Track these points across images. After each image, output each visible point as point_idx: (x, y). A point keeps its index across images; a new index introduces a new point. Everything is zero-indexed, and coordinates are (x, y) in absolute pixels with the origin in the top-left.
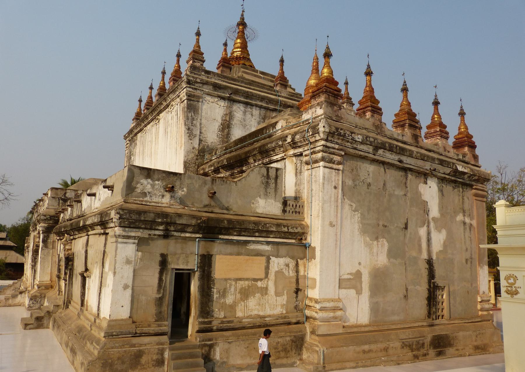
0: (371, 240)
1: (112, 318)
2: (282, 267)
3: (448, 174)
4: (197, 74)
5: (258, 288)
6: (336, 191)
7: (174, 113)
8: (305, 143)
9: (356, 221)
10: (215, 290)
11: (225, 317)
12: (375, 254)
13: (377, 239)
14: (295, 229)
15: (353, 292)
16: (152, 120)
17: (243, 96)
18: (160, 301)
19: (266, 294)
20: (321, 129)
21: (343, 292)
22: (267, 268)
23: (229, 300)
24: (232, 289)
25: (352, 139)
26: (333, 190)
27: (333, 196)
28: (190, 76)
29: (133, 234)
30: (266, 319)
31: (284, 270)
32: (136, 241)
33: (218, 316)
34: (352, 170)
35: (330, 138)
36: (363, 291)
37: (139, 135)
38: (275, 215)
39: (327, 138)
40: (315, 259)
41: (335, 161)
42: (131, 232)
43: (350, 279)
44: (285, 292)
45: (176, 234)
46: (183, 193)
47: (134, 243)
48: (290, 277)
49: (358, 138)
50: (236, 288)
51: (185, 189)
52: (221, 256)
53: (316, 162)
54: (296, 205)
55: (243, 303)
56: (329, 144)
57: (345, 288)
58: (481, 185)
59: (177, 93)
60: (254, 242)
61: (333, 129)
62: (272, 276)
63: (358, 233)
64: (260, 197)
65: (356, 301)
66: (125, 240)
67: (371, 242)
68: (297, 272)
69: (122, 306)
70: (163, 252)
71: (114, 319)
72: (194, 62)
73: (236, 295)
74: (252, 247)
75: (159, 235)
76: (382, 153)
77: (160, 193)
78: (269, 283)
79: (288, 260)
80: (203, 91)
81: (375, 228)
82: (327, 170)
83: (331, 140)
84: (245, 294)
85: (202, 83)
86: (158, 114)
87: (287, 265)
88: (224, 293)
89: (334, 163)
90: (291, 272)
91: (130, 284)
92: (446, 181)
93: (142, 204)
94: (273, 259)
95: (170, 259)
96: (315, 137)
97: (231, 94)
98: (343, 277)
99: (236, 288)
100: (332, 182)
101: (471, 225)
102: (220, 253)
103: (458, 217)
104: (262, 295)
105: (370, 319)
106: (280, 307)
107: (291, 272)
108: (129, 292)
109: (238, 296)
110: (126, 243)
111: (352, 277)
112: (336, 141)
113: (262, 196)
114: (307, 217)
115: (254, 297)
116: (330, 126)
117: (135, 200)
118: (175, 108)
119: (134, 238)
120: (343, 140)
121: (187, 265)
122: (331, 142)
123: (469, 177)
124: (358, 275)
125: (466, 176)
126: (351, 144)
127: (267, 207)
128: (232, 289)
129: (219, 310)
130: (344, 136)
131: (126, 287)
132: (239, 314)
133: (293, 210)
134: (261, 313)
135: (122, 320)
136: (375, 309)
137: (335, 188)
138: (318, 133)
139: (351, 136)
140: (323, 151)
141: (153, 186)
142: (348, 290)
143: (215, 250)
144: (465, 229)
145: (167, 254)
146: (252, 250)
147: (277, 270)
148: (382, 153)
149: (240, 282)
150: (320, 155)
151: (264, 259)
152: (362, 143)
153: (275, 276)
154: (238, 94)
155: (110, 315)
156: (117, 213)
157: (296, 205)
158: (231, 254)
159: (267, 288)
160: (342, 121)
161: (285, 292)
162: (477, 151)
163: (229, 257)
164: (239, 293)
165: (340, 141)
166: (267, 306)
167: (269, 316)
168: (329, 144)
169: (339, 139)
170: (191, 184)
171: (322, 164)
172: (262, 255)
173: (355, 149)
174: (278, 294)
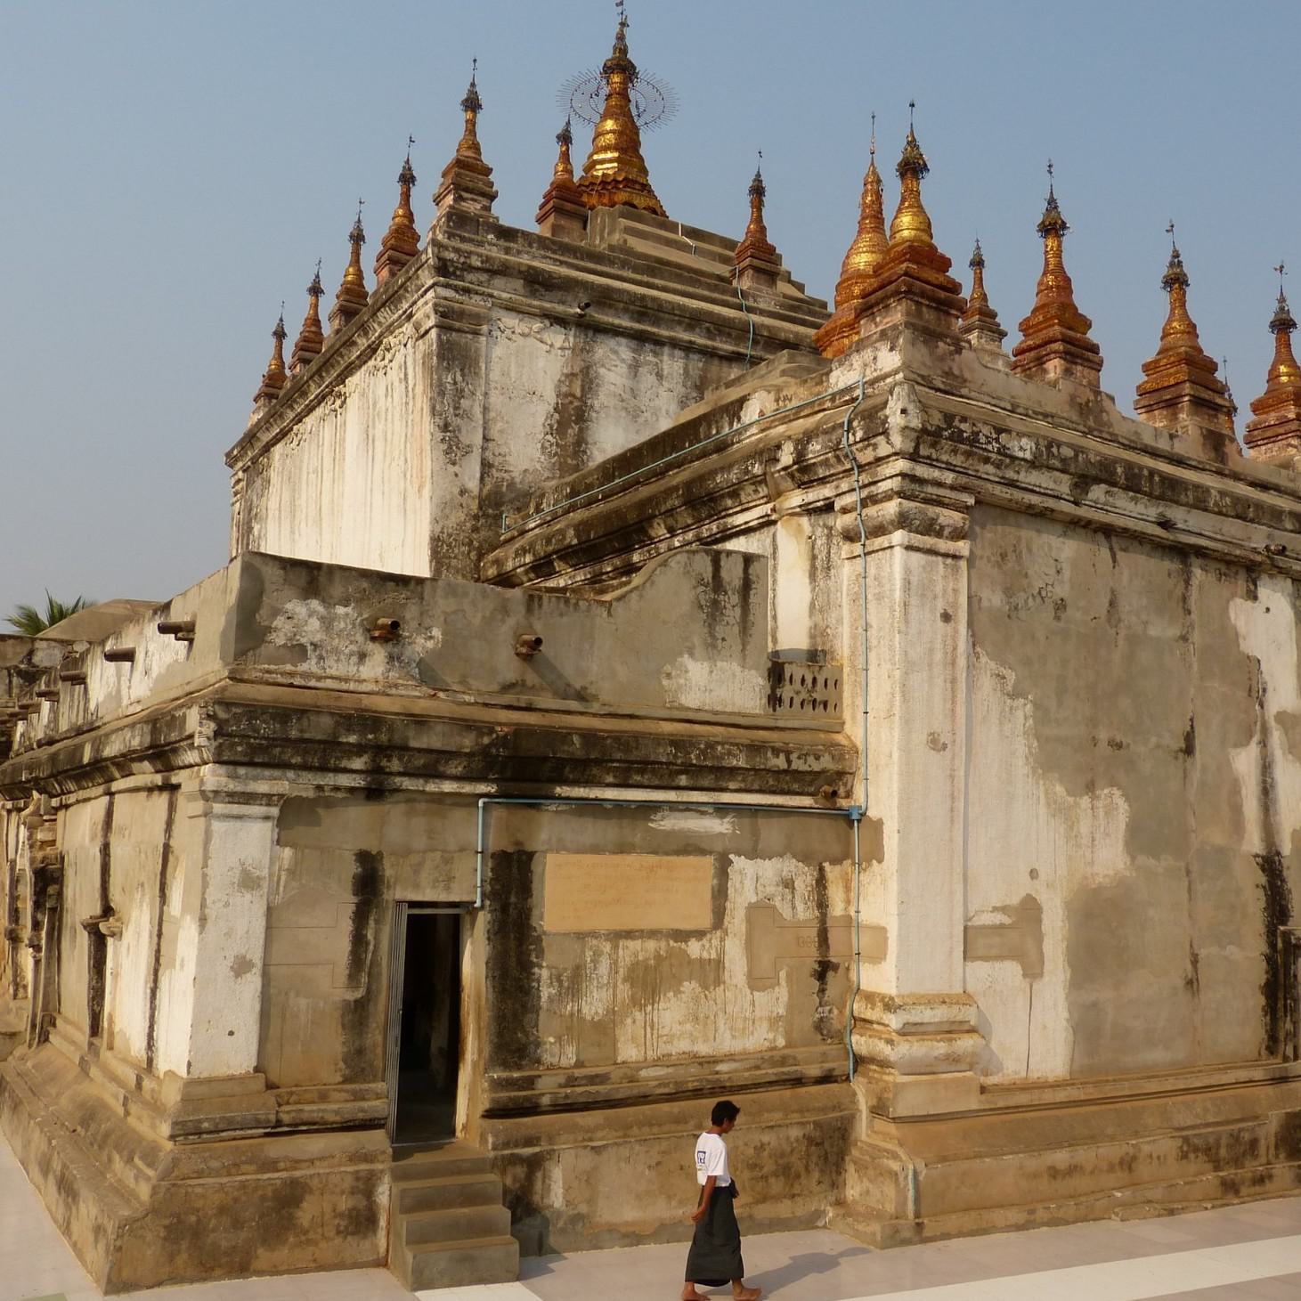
2: (771, 890)
4: (471, 241)
5: (690, 962)
6: (949, 628)
7: (394, 374)
8: (840, 468)
10: (545, 973)
12: (1085, 841)
13: (1090, 788)
14: (811, 759)
16: (321, 399)
17: (626, 310)
18: (357, 1014)
19: (718, 981)
22: (720, 895)
23: (594, 1004)
24: (604, 967)
25: (999, 453)
26: (940, 624)
27: (938, 645)
28: (446, 248)
29: (262, 787)
30: (721, 1067)
31: (777, 902)
32: (275, 811)
34: (1003, 556)
35: (924, 451)
36: (1048, 966)
37: (278, 450)
40: (880, 861)
41: (942, 528)
43: (1002, 926)
44: (783, 974)
45: (407, 783)
46: (430, 644)
47: (267, 818)
49: (1021, 448)
51: (436, 632)
52: (563, 857)
53: (880, 530)
54: (814, 680)
55: (639, 1016)
56: (922, 471)
57: (986, 959)
60: (674, 807)
61: (937, 419)
62: (736, 920)
65: (1022, 1002)
66: (236, 809)
67: (1071, 799)
69: (231, 1033)
70: (364, 846)
72: (459, 199)
73: (615, 987)
75: (352, 790)
77: (353, 648)
80: (491, 296)
81: (1084, 755)
83: (929, 458)
84: (648, 984)
86: (341, 379)
87: (789, 884)
88: (574, 983)
89: (939, 534)
90: (800, 907)
91: (256, 956)
93: (291, 685)
94: (739, 862)
96: (875, 446)
97: (587, 305)
100: (935, 597)
102: (561, 847)
104: (705, 987)
105: (1072, 1060)
106: (765, 1025)
107: (800, 907)
108: (253, 981)
109: (624, 991)
111: (1007, 920)
112: (944, 458)
113: (699, 651)
114: (854, 718)
118: (399, 358)
119: (268, 799)
120: (968, 454)
122: (931, 462)
124: (1029, 911)
126: (998, 467)
127: (715, 685)
128: (604, 967)
129: (559, 1039)
130: (973, 440)
132: (628, 1052)
133: (804, 695)
134: (703, 1049)
135: (231, 1078)
137: (946, 617)
139: (997, 440)
140: (901, 494)
148: (1102, 499)
151: (709, 861)
152: (1033, 464)
154: (610, 306)
155: (189, 1064)
156: (209, 717)
157: (814, 680)
158: (596, 849)
159: (719, 964)
160: (964, 391)
161: (783, 974)
163: (589, 859)
164: (625, 980)
165: (958, 460)
167: (730, 1057)
168: (922, 471)
169: (955, 451)
171: (898, 536)
172: (702, 852)
173: (1012, 484)
174: (757, 982)
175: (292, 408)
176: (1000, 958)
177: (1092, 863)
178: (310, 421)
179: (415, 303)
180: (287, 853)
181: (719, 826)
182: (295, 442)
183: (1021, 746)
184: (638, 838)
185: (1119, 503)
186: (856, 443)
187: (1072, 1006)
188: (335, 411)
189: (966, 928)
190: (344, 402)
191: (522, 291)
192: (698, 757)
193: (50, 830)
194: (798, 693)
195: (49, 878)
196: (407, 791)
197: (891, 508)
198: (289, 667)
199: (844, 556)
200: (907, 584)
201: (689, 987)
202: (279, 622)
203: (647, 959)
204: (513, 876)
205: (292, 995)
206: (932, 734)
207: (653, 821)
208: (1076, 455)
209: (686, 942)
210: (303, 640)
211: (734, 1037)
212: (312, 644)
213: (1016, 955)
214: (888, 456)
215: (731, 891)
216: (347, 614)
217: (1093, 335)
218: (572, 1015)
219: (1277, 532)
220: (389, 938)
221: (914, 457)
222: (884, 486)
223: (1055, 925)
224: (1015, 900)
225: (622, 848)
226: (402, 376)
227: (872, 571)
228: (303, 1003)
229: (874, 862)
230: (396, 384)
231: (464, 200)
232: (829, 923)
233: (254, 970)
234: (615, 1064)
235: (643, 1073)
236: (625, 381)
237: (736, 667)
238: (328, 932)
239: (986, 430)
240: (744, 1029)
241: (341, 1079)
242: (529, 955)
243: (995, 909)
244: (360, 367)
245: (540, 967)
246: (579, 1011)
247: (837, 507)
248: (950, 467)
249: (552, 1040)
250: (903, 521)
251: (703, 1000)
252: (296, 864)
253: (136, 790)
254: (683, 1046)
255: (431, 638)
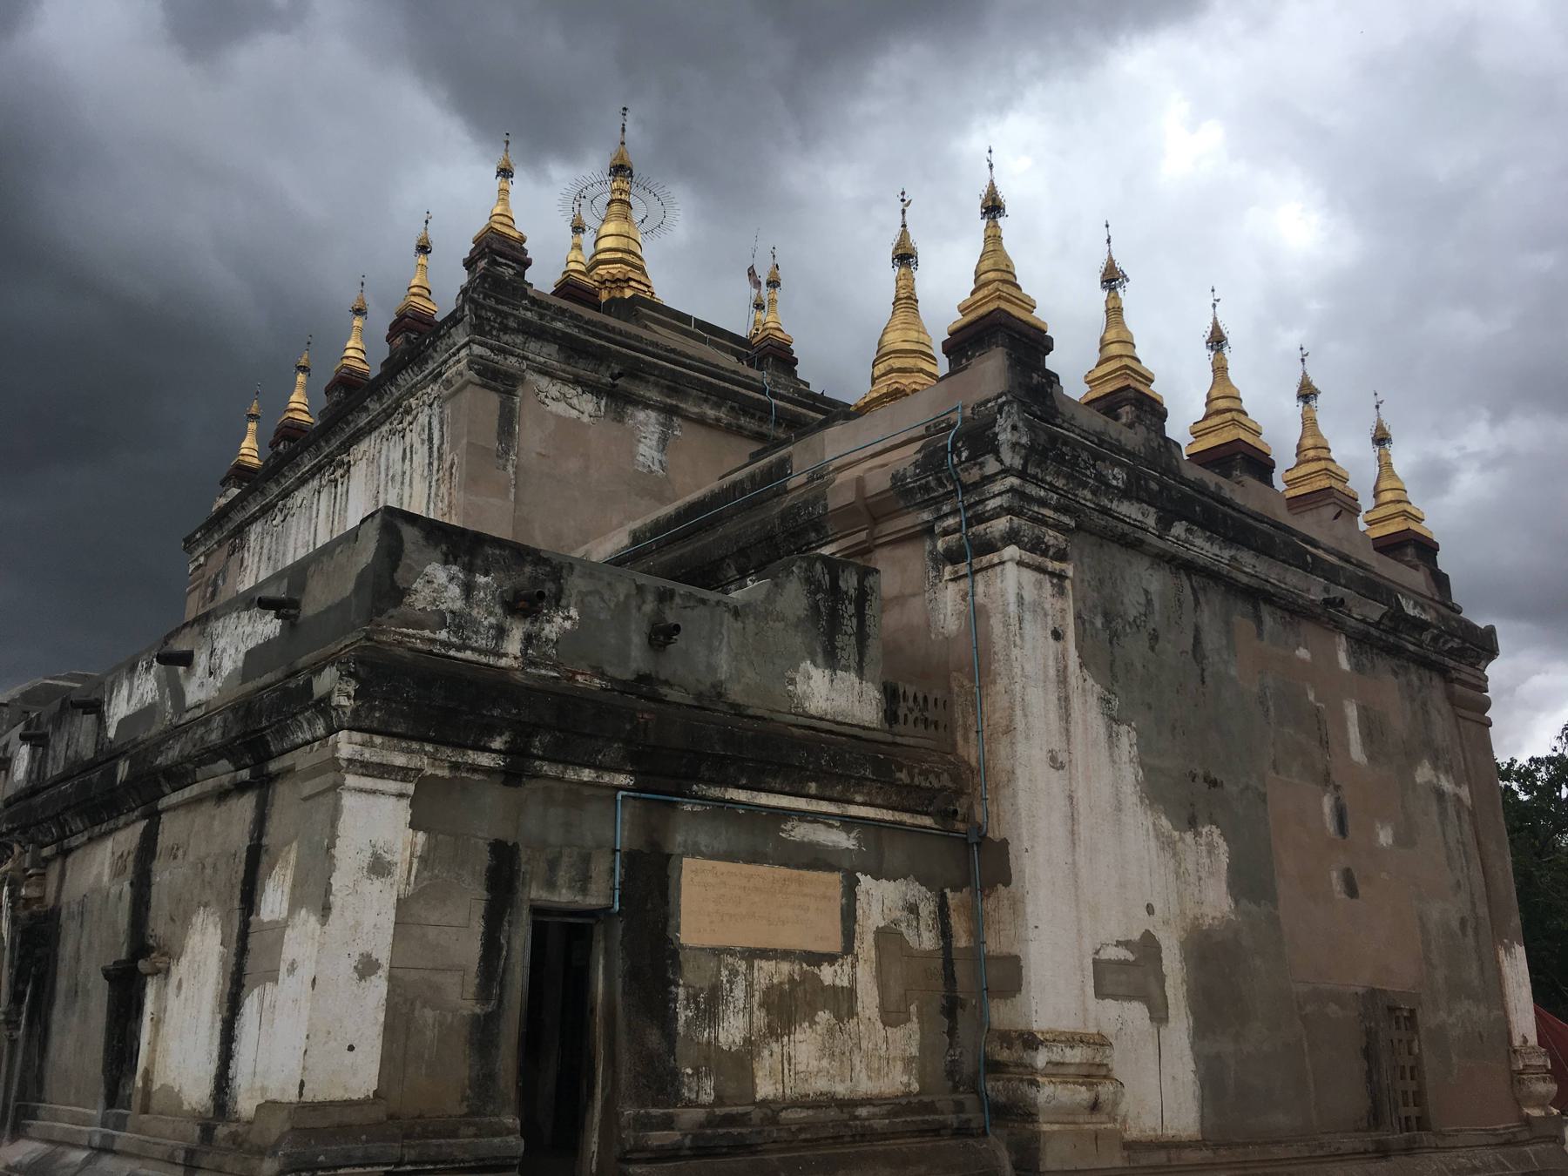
0: (1175, 828)
1: (308, 1096)
2: (898, 914)
3: (1377, 625)
4: (507, 304)
5: (824, 988)
6: (1059, 645)
7: (413, 437)
8: (941, 491)
9: (1125, 758)
10: (681, 992)
11: (720, 1100)
12: (1193, 879)
13: (1192, 824)
14: (932, 777)
15: (1136, 1012)
16: (318, 470)
17: (656, 385)
18: (483, 1032)
19: (852, 1013)
20: (1005, 437)
21: (1112, 1008)
22: (849, 916)
23: (732, 1030)
24: (739, 992)
25: (1095, 479)
26: (1051, 641)
27: (1051, 662)
28: (483, 307)
29: (400, 760)
30: (863, 1112)
31: (903, 927)
32: (410, 788)
33: (693, 1096)
34: (1101, 581)
35: (1031, 470)
36: (1171, 1012)
37: (256, 528)
38: (864, 728)
39: (1025, 466)
40: (1007, 883)
41: (1048, 547)
42: (393, 749)
43: (1125, 963)
44: (913, 1008)
45: (548, 768)
46: (568, 624)
47: (401, 796)
48: (928, 955)
49: (1115, 477)
50: (750, 985)
51: (573, 613)
52: (699, 863)
53: (988, 547)
54: (925, 699)
55: (776, 1047)
56: (1032, 490)
57: (1115, 997)
58: (1469, 670)
59: (431, 366)
60: (803, 816)
61: (1043, 438)
62: (866, 946)
63: (1135, 799)
64: (814, 663)
65: (1151, 1049)
66: (368, 783)
67: (1176, 834)
68: (946, 933)
69: (351, 1048)
70: (500, 836)
71: (320, 1098)
72: (494, 263)
73: (751, 1014)
74: (801, 832)
75: (488, 771)
76: (1183, 536)
77: (492, 620)
78: (859, 970)
79: (913, 890)
80: (526, 358)
81: (1188, 792)
82: (1028, 576)
83: (1035, 476)
84: (784, 1010)
85: (524, 333)
86: (346, 447)
87: (913, 909)
88: (711, 1006)
89: (1044, 553)
90: (926, 935)
91: (383, 955)
92: (1372, 646)
93: (430, 652)
94: (865, 881)
95: (527, 862)
96: (982, 465)
97: (620, 375)
98: (1104, 955)
99: (750, 985)
100: (1046, 615)
101: (1458, 799)
102: (696, 853)
103: (1419, 771)
104: (839, 1019)
105: (1202, 1116)
106: (899, 1065)
107: (926, 935)
108: (379, 987)
109: (760, 1018)
110: (374, 792)
111: (1131, 957)
112: (1049, 479)
113: (820, 660)
114: (966, 739)
115: (813, 1023)
116: (1031, 428)
117: (408, 635)
118: (423, 419)
119: (403, 774)
120: (1069, 477)
121: (584, 890)
122: (1038, 482)
123: (1435, 639)
124: (1148, 947)
125: (1427, 637)
126: (1094, 493)
127: (831, 694)
128: (739, 992)
129: (697, 1072)
130: (1074, 464)
131: (366, 967)
132: (765, 1088)
133: (917, 713)
134: (841, 1089)
135: (349, 1103)
136: (1213, 1081)
137: (1057, 635)
138: (996, 451)
139: (1094, 466)
140: (1009, 511)
141: (468, 589)
142: (1126, 1004)
143: (679, 838)
144: (1443, 813)
145: (516, 845)
146: (802, 846)
147: (882, 924)
148: (1183, 536)
149: (764, 964)
150: (1001, 525)
151: (837, 877)
152: (1125, 494)
153: (877, 947)
154: (641, 379)
155: (302, 1085)
156: (350, 675)
157: (925, 699)
158: (730, 857)
159: (851, 993)
160: (1059, 421)
161: (913, 1008)
162: (1444, 562)
163: (722, 866)
164: (761, 1005)
165: (1060, 483)
166: (856, 1059)
167: (867, 1101)
168: (1032, 490)
169: (1058, 474)
170: (590, 593)
171: (1011, 551)
172: (831, 868)
173: (1105, 511)
174: (891, 1016)
175: (278, 483)
176: (1129, 998)
177: (1200, 903)
178: (301, 495)
179: (445, 362)
180: (421, 837)
181: (842, 840)
182: (279, 518)
183: (1130, 774)
184: (769, 849)
185: (1198, 542)
186: (961, 463)
187: (1197, 1058)
188: (336, 481)
189: (1095, 962)
190: (348, 471)
191: (555, 355)
192: (828, 762)
193: (38, 885)
194: (911, 710)
195: (39, 935)
196: (546, 777)
197: (1001, 525)
198: (427, 633)
199: (947, 577)
200: (1020, 598)
201: (823, 1016)
202: (418, 584)
203: (781, 983)
204: (650, 882)
205: (418, 1004)
206: (1051, 751)
207: (784, 831)
208: (1160, 492)
209: (819, 966)
210: (443, 607)
211: (870, 1078)
212: (452, 612)
213: (1145, 998)
214: (996, 474)
215: (859, 912)
216: (487, 583)
217: (1156, 388)
218: (709, 1043)
219: (1332, 586)
220: (519, 941)
221: (1022, 474)
222: (992, 504)
223: (1172, 963)
224: (1136, 936)
225: (755, 858)
226: (425, 437)
227: (980, 589)
228: (429, 1014)
229: (1000, 886)
230: (417, 445)
231: (500, 264)
232: (955, 955)
233: (380, 972)
234: (754, 1103)
235: (783, 1114)
236: (656, 454)
237: (853, 676)
238: (460, 935)
239: (1085, 455)
240: (879, 1069)
241: (466, 1110)
242: (666, 971)
243: (1119, 943)
244: (370, 433)
245: (678, 985)
246: (716, 1038)
247: (937, 530)
248: (1053, 488)
249: (689, 1071)
250: (1012, 537)
251: (838, 1034)
252: (429, 851)
253: (198, 800)
254: (820, 1085)
255: (569, 618)
